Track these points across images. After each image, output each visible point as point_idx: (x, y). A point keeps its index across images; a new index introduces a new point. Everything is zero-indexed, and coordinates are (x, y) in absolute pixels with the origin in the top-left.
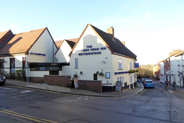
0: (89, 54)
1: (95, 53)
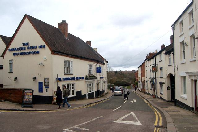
0: (25, 53)
1: (33, 53)
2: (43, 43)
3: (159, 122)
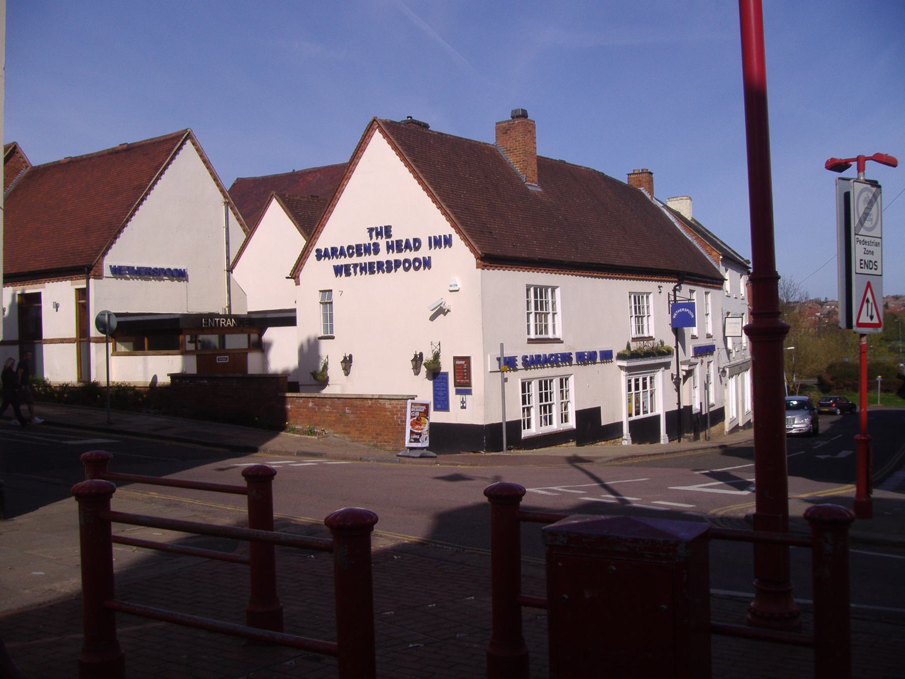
1: (408, 265)
2: (444, 227)
3: (489, 552)
